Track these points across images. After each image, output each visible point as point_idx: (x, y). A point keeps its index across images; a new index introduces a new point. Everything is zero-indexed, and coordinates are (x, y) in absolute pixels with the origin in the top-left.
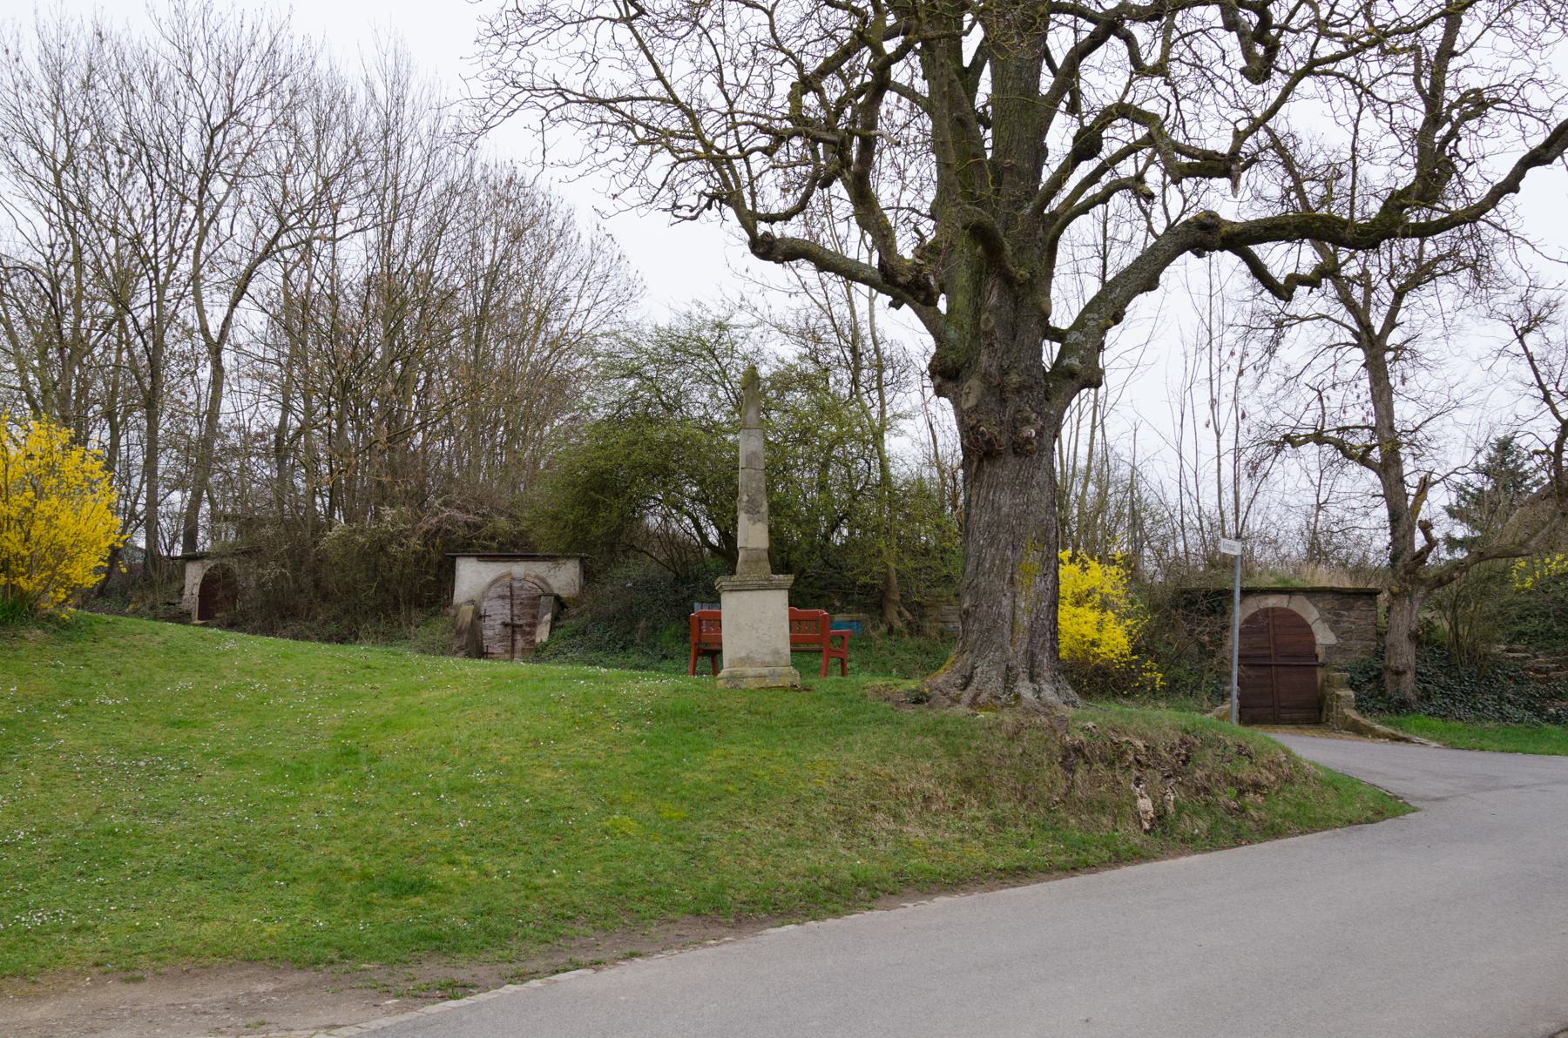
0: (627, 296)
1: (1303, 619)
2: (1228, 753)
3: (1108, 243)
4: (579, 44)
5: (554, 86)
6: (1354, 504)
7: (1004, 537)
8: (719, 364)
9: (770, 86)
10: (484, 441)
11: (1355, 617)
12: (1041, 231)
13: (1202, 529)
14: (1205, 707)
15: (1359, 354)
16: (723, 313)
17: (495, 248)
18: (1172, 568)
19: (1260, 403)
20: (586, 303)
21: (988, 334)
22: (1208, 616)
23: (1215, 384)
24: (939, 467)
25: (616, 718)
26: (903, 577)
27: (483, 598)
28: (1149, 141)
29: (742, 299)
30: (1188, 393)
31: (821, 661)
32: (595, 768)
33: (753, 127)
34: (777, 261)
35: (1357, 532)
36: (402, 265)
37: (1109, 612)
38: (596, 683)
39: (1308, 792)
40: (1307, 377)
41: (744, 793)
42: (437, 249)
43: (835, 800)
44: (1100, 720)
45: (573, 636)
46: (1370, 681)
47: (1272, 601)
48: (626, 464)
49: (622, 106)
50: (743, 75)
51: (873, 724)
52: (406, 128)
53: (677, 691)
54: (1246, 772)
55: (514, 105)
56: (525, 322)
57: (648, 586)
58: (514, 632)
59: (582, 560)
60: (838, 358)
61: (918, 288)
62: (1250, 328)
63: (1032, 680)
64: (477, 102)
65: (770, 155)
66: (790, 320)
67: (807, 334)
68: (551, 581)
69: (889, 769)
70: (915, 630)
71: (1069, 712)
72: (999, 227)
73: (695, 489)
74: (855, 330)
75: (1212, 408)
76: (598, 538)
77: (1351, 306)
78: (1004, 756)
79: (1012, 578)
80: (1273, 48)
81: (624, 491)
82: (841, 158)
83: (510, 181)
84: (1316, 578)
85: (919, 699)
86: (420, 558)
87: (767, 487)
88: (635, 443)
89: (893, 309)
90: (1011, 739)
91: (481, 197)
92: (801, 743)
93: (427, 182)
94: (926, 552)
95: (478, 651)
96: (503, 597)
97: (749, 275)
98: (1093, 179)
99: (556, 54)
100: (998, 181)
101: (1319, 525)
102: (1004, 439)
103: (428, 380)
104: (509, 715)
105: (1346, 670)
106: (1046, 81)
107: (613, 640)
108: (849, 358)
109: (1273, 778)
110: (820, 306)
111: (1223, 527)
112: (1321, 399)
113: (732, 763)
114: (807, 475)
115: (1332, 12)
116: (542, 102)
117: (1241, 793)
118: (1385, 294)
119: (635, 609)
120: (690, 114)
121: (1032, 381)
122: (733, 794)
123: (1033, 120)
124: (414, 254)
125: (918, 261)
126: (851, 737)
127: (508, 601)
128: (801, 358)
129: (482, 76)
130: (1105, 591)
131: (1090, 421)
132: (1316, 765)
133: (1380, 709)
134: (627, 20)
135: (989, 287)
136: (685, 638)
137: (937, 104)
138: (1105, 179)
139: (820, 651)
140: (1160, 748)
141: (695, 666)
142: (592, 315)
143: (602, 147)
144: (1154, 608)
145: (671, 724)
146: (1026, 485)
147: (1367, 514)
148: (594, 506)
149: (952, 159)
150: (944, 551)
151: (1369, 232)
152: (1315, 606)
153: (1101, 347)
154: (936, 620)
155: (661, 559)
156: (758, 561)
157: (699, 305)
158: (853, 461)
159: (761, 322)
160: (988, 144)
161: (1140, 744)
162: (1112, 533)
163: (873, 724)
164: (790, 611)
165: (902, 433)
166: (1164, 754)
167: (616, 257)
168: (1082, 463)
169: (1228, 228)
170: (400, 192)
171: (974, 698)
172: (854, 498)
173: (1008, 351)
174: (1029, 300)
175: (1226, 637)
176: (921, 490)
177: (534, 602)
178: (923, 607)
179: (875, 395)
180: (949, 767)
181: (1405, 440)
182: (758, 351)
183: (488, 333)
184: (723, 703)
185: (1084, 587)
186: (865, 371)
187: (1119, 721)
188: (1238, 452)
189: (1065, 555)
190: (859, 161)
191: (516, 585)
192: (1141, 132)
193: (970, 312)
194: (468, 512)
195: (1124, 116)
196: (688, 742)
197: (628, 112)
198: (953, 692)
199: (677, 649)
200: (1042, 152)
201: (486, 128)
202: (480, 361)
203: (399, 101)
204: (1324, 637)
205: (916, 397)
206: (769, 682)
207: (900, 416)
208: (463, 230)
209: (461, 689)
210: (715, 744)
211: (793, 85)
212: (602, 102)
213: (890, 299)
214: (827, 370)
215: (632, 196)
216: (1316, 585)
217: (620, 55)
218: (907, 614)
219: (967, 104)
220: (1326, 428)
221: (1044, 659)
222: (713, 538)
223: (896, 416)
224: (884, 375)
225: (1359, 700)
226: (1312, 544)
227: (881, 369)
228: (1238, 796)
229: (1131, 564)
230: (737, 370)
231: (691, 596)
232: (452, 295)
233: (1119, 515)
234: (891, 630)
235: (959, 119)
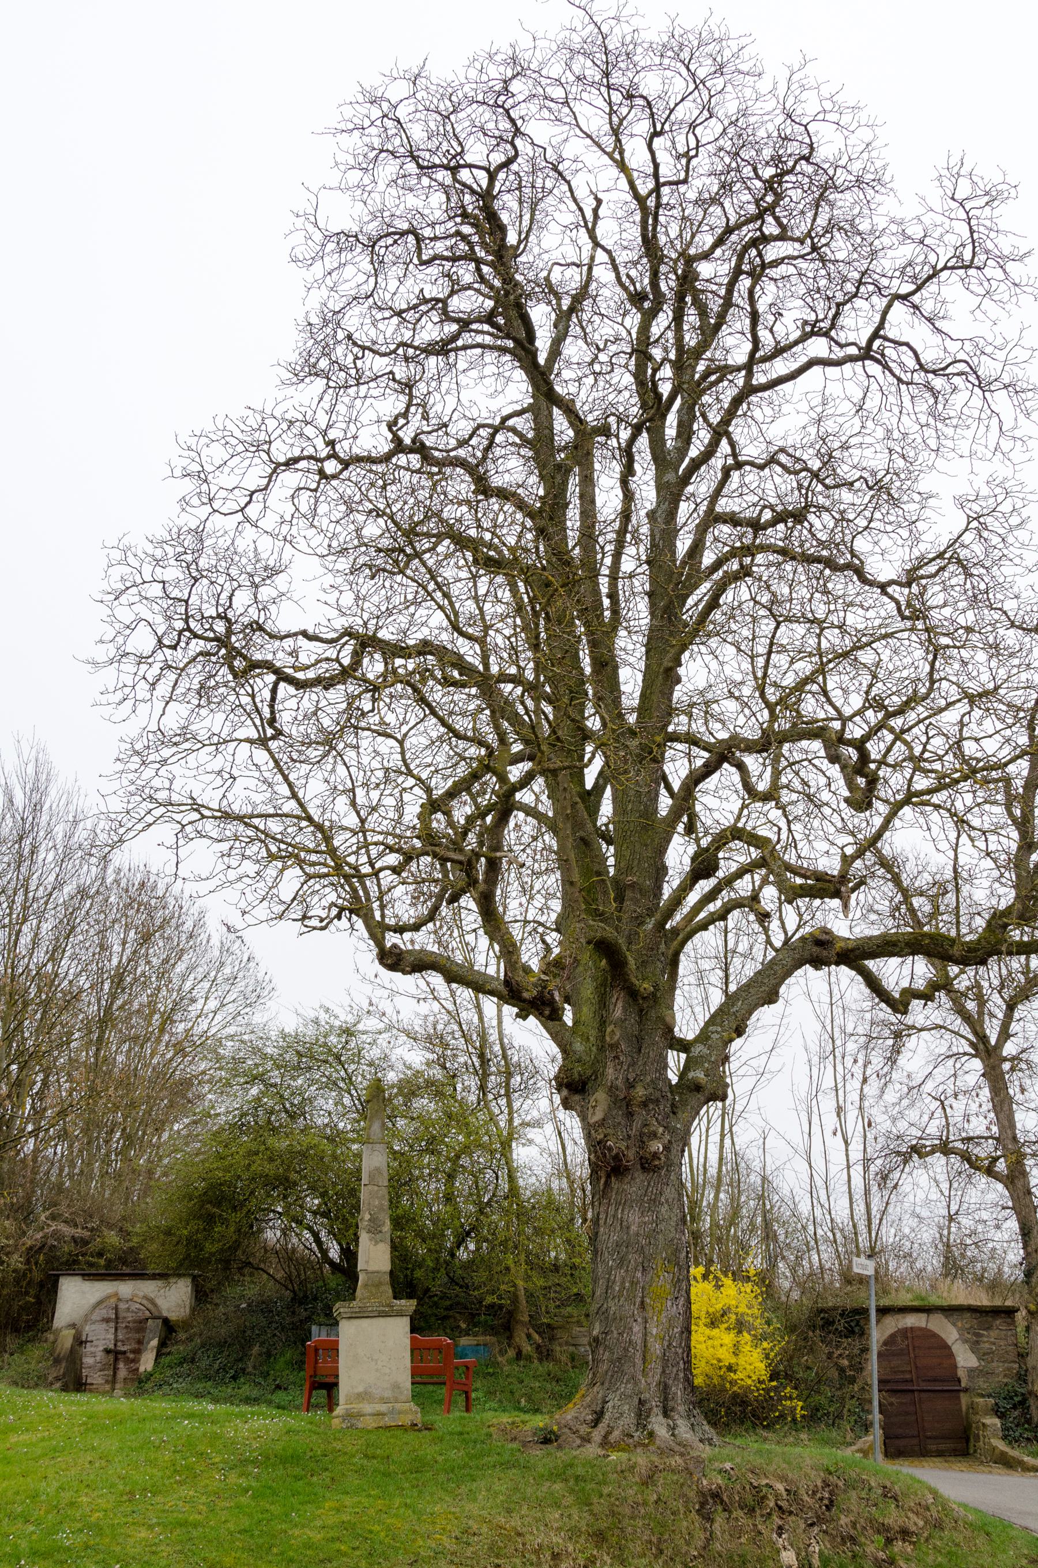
0: (254, 998)
1: (942, 1340)
2: (873, 1496)
3: (729, 955)
4: (217, 763)
5: (190, 801)
6: (985, 1215)
7: (633, 1258)
9: (400, 808)
10: (99, 1148)
11: (995, 1336)
12: (663, 946)
13: (835, 1241)
14: (848, 1439)
15: (977, 1064)
16: (350, 1019)
17: (123, 950)
18: (807, 1283)
19: (885, 1112)
20: (212, 1004)
21: (614, 1046)
22: (846, 1337)
23: (841, 1093)
24: (568, 1178)
25: (221, 1466)
26: (532, 1295)
27: (86, 1321)
28: (761, 863)
29: (371, 1004)
30: (814, 1102)
31: (444, 1391)
32: (195, 1526)
33: (382, 847)
34: (404, 972)
35: (990, 1245)
36: (27, 966)
37: (745, 1334)
38: (202, 1423)
39: (959, 1538)
40: (929, 1087)
41: (358, 1553)
42: (64, 951)
43: (456, 1560)
44: (738, 1460)
45: (181, 1364)
46: (1015, 1407)
47: (911, 1321)
49: (256, 821)
50: (375, 795)
52: (42, 834)
53: (288, 1432)
54: (893, 1517)
55: (149, 819)
56: (150, 1024)
57: (264, 1307)
58: (116, 1360)
59: (194, 1278)
60: (466, 1063)
61: (544, 1003)
62: (870, 1038)
63: (666, 1415)
64: (113, 816)
65: (399, 874)
66: (417, 1026)
67: (435, 1040)
68: (160, 1302)
69: (516, 1522)
70: (545, 1354)
71: (706, 1451)
72: (622, 941)
73: (316, 1202)
74: (483, 1036)
75: (839, 1115)
76: (212, 1254)
77: (967, 1017)
78: (638, 1504)
79: (642, 1302)
80: (873, 781)
81: (242, 1204)
82: (468, 875)
83: (143, 885)
84: (952, 1295)
85: (547, 1439)
86: (20, 1277)
88: (257, 1153)
90: (645, 1484)
91: (112, 899)
92: (420, 1492)
93: (58, 885)
94: (556, 1268)
95: (76, 1384)
96: (107, 1320)
97: (378, 980)
98: (710, 897)
99: (194, 772)
100: (620, 898)
101: (952, 1237)
102: (631, 1154)
103: (45, 1083)
104: (104, 1463)
105: (989, 1396)
106: (665, 803)
107: (224, 1369)
108: (477, 1064)
109: (921, 1523)
110: (448, 1012)
111: (857, 1240)
112: (944, 1108)
113: (345, 1518)
114: (433, 1186)
115: (924, 750)
116: (178, 817)
117: (889, 1541)
118: (997, 1004)
119: (249, 1333)
120: (319, 827)
121: (658, 1094)
122: (345, 1555)
123: (653, 840)
124: (40, 955)
125: (543, 977)
126: (475, 1485)
127: (112, 1324)
128: (428, 1064)
129: (120, 793)
130: (740, 1310)
131: (719, 1129)
132: (965, 1506)
133: (1028, 1439)
134: (263, 742)
135: (614, 1000)
136: (300, 1365)
137: (561, 825)
138: (725, 895)
139: (444, 1383)
140: (802, 1491)
141: (310, 1397)
142: (219, 1017)
143: (234, 863)
144: (791, 1329)
145: (280, 1472)
146: (655, 1202)
147: (998, 1227)
148: (210, 1220)
149: (576, 877)
150: (574, 1267)
151: (976, 950)
152: (954, 1325)
153: (726, 1059)
154: (567, 1343)
155: (278, 1276)
156: (378, 1285)
157: (327, 1010)
158: (480, 1171)
159: (389, 1028)
160: (611, 861)
161: (780, 1487)
162: (745, 1248)
164: (413, 1339)
165: (531, 1142)
166: (806, 1498)
167: (245, 959)
168: (712, 1171)
169: (842, 944)
170: (31, 894)
171: (605, 1437)
172: (481, 1211)
173: (633, 1064)
174: (653, 1014)
175: (867, 1360)
176: (550, 1202)
177: (140, 1325)
178: (553, 1329)
179: (503, 1102)
180: (580, 1518)
181: (1028, 1151)
182: (386, 1058)
183: (111, 1035)
184: (338, 1445)
185: (719, 1307)
186: (493, 1077)
187: (759, 1461)
188: (867, 1162)
189: (697, 1271)
190: (485, 881)
191: (122, 1306)
192: (755, 853)
193: (596, 1025)
194: (76, 1226)
195: (739, 839)
196: (299, 1493)
197: (262, 827)
198: (584, 1429)
199: (292, 1378)
200: (661, 871)
201: (121, 841)
202: (99, 1067)
203: (37, 808)
204: (965, 1359)
205: (544, 1104)
206: (387, 1421)
207: (528, 1125)
208: (92, 932)
209: (53, 1431)
210: (328, 1495)
211: (422, 806)
212: (240, 818)
213: (515, 1010)
214: (454, 1076)
215: (262, 911)
216: (954, 1303)
217: (257, 774)
218: (536, 1336)
219: (589, 825)
220: (952, 1138)
221: (678, 1390)
222: (334, 1253)
223: (525, 1124)
225: (1005, 1429)
226: (947, 1258)
227: (509, 1075)
228: (886, 1545)
229: (766, 1281)
231: (309, 1319)
232: (76, 997)
233: (752, 1228)
234: (519, 1355)
235: (582, 839)
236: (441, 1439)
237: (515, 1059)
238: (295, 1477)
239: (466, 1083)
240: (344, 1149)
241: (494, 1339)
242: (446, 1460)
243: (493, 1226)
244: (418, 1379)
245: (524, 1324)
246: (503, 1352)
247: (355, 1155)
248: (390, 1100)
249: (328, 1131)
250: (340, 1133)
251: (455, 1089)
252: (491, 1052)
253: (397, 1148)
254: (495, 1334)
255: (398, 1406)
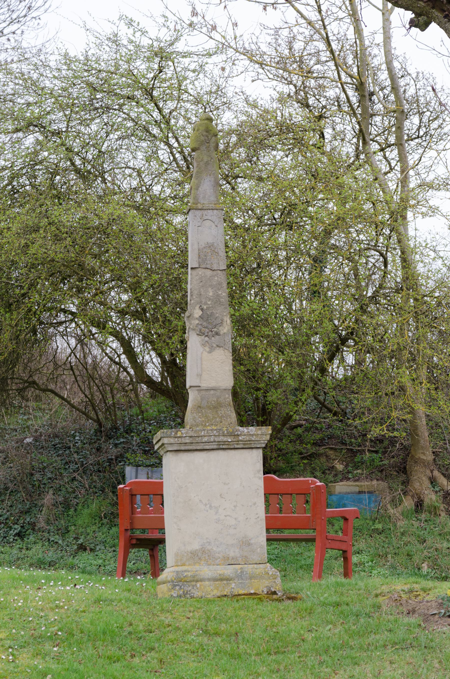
8: (160, 110)
25: (8, 643)
29: (194, 13)
48: (23, 260)
51: (389, 650)
53: (97, 601)
60: (338, 99)
73: (125, 297)
87: (231, 296)
89: (415, 30)
108: (354, 100)
110: (310, 23)
114: (292, 274)
119: (37, 476)
126: (358, 669)
139: (313, 540)
155: (75, 401)
156: (217, 406)
157: (130, 23)
158: (360, 253)
163: (389, 650)
165: (434, 210)
172: (363, 309)
179: (393, 154)
184: (167, 618)
186: (378, 119)
199: (100, 536)
207: (430, 186)
213: (409, 15)
224: (407, 123)
230: (188, 120)
231: (120, 458)
236: (310, 612)
237: (411, 91)
238: (109, 658)
239: (339, 128)
240: (162, 222)
241: (383, 485)
242: (317, 639)
243: (381, 330)
244: (274, 534)
245: (425, 464)
246: (395, 502)
247: (177, 231)
248: (227, 153)
249: (138, 198)
250: (155, 199)
251: (322, 136)
252: (375, 81)
253: (238, 221)
254: (385, 478)
255: (249, 568)
